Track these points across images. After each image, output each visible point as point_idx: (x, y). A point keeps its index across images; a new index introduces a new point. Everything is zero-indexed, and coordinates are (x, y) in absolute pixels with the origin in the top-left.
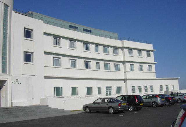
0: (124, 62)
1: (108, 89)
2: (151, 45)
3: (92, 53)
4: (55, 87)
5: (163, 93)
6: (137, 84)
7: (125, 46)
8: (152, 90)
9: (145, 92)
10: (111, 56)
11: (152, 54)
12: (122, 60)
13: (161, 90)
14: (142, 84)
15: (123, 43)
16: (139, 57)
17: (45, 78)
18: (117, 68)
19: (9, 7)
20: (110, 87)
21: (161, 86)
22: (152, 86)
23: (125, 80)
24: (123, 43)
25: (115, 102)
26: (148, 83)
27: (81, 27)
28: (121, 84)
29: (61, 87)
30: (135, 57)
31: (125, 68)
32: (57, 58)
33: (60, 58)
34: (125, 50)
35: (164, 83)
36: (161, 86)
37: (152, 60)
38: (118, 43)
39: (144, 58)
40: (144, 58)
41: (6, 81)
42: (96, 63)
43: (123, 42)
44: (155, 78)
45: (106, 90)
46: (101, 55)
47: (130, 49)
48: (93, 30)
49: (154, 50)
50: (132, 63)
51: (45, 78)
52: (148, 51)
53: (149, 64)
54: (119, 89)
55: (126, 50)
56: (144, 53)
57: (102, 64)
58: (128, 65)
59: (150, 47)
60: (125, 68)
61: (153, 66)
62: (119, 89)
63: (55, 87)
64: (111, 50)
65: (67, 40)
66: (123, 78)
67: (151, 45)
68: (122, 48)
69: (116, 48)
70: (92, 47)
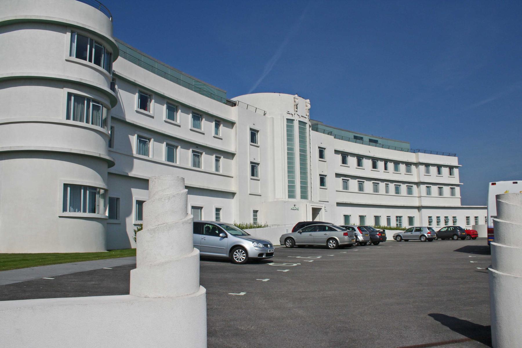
0: (418, 184)
1: (399, 218)
2: (456, 159)
3: (380, 173)
4: (66, 186)
5: (471, 229)
6: (434, 213)
7: (421, 161)
8: (454, 222)
9: (438, 225)
10: (402, 175)
11: (456, 171)
12: (416, 180)
13: (468, 223)
14: (442, 213)
15: (417, 157)
16: (395, 172)
17: (337, 206)
18: (410, 191)
19: (307, 123)
20: (400, 217)
21: (468, 218)
22: (454, 217)
23: (419, 208)
24: (417, 157)
25: (336, 230)
26: (450, 214)
27: (366, 139)
28: (414, 213)
29: (365, 216)
30: (433, 176)
31: (420, 192)
32: (345, 178)
33: (412, 186)
34: (420, 166)
35: (472, 213)
36: (468, 218)
37: (455, 180)
38: (411, 157)
39: (445, 177)
40: (445, 177)
41: (321, 209)
42: (385, 185)
43: (418, 154)
44: (459, 205)
45: (397, 220)
46: (391, 175)
47: (427, 165)
48: (380, 141)
49: (461, 166)
50: (429, 185)
51: (337, 206)
52: (451, 168)
53: (452, 186)
54: (411, 220)
55: (422, 168)
56: (445, 171)
57: (392, 186)
58: (423, 187)
59: (453, 161)
60: (420, 192)
61: (457, 190)
62: (411, 220)
63: (66, 186)
64: (402, 167)
65: (435, 167)
66: (417, 204)
67: (456, 159)
68: (417, 164)
69: (408, 164)
70: (381, 165)
